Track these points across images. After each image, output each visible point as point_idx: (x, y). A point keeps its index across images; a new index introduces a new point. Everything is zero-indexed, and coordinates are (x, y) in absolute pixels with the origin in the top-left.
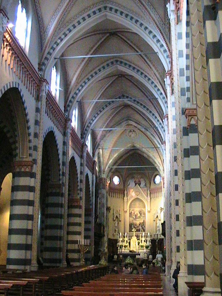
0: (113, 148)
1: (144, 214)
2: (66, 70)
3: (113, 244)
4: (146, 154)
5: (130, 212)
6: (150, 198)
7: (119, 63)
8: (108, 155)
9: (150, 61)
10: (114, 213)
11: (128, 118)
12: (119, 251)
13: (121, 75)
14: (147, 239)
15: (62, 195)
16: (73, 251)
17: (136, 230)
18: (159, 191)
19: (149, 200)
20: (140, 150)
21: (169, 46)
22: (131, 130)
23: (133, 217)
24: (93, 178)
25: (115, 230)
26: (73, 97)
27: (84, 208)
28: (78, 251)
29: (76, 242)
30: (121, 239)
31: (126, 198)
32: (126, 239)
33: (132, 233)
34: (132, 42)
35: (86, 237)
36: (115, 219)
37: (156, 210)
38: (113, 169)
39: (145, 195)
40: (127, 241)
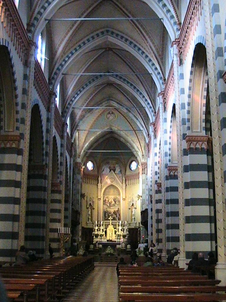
0: (90, 129)
1: (119, 202)
2: (52, 38)
3: (88, 233)
4: (124, 139)
5: (104, 199)
6: (125, 185)
7: (109, 33)
8: (83, 139)
9: (146, 32)
10: (88, 200)
11: (110, 98)
12: (95, 240)
13: (109, 48)
14: (124, 227)
15: (45, 177)
16: (53, 240)
17: (112, 218)
18: (129, 179)
19: (124, 188)
20: (116, 134)
21: (177, 12)
22: (110, 112)
23: (107, 205)
24: (70, 161)
25: (88, 219)
26: (58, 69)
27: (63, 192)
28: (58, 240)
29: (56, 230)
30: (97, 228)
31: (100, 185)
32: (102, 228)
33: (108, 221)
34: (127, 10)
35: (65, 225)
36: (88, 207)
37: (131, 198)
38: (88, 153)
39: (120, 183)
40: (103, 230)
